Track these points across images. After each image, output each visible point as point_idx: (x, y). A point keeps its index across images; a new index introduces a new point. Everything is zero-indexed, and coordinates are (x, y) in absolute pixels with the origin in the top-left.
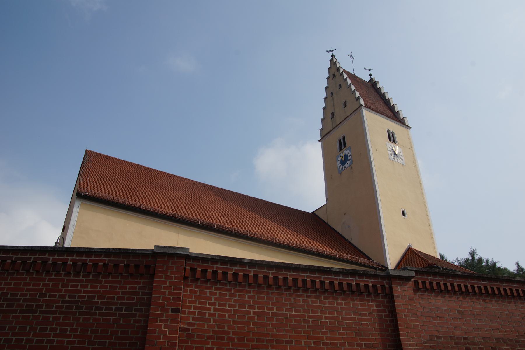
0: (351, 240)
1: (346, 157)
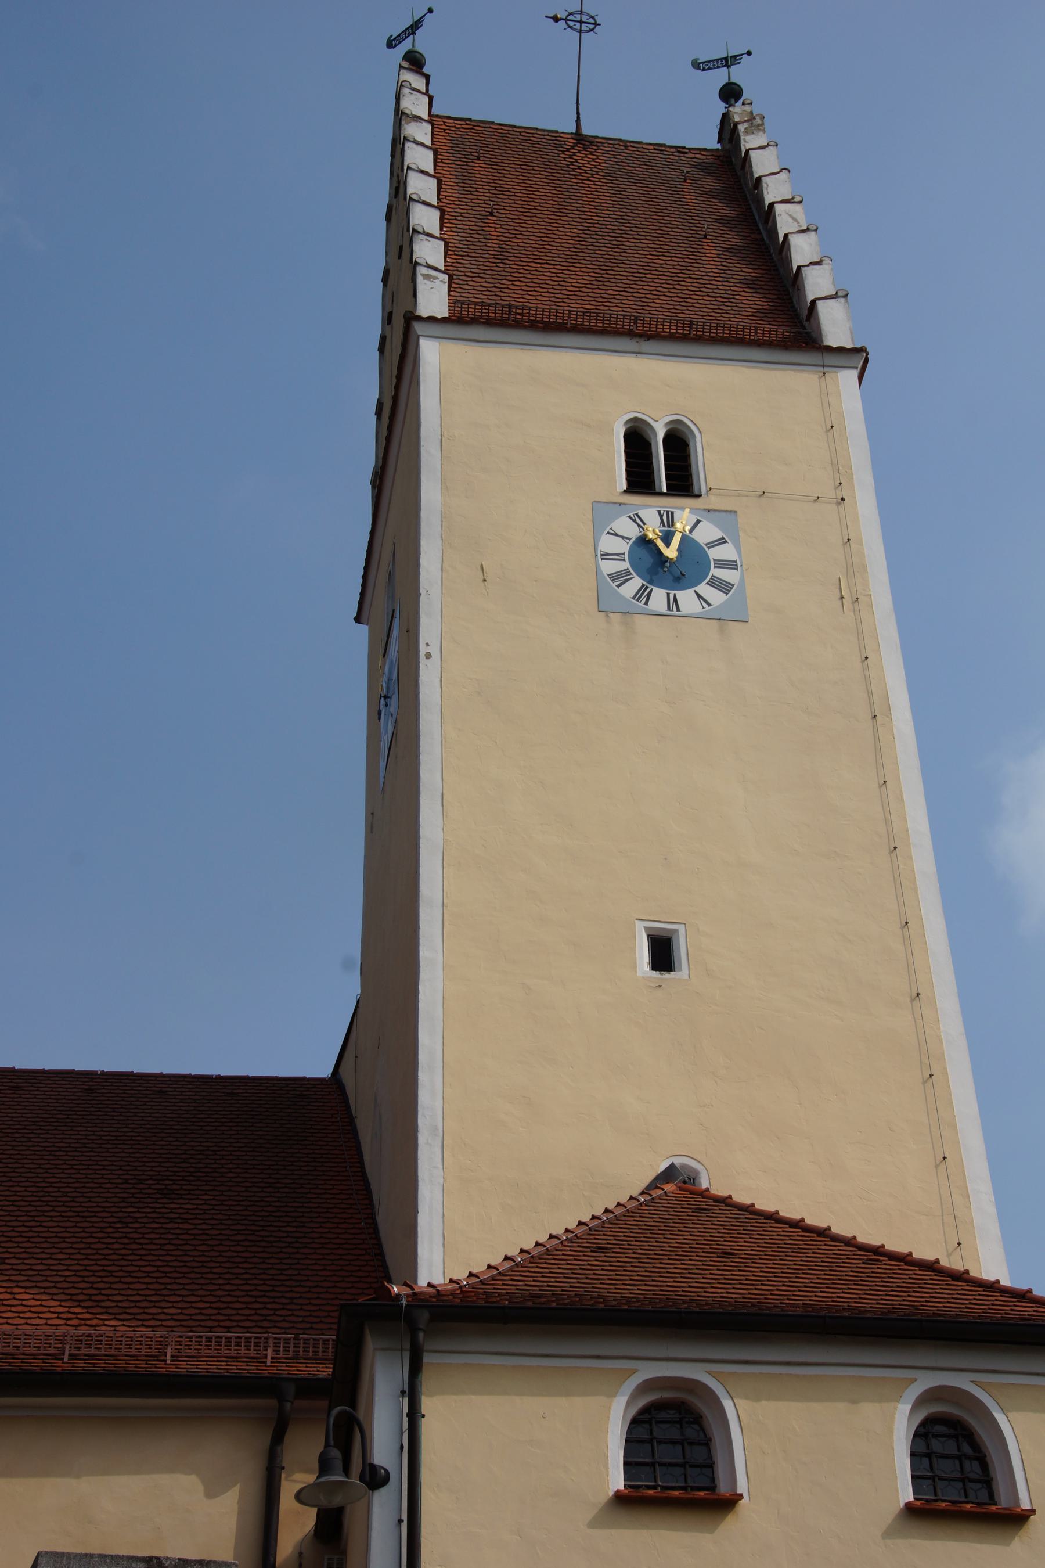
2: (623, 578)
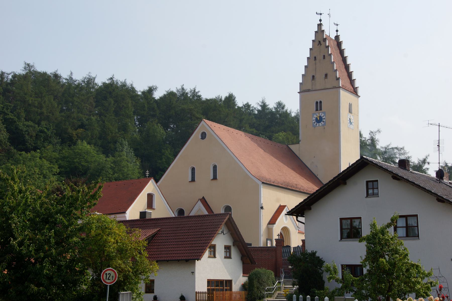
0: (317, 175)
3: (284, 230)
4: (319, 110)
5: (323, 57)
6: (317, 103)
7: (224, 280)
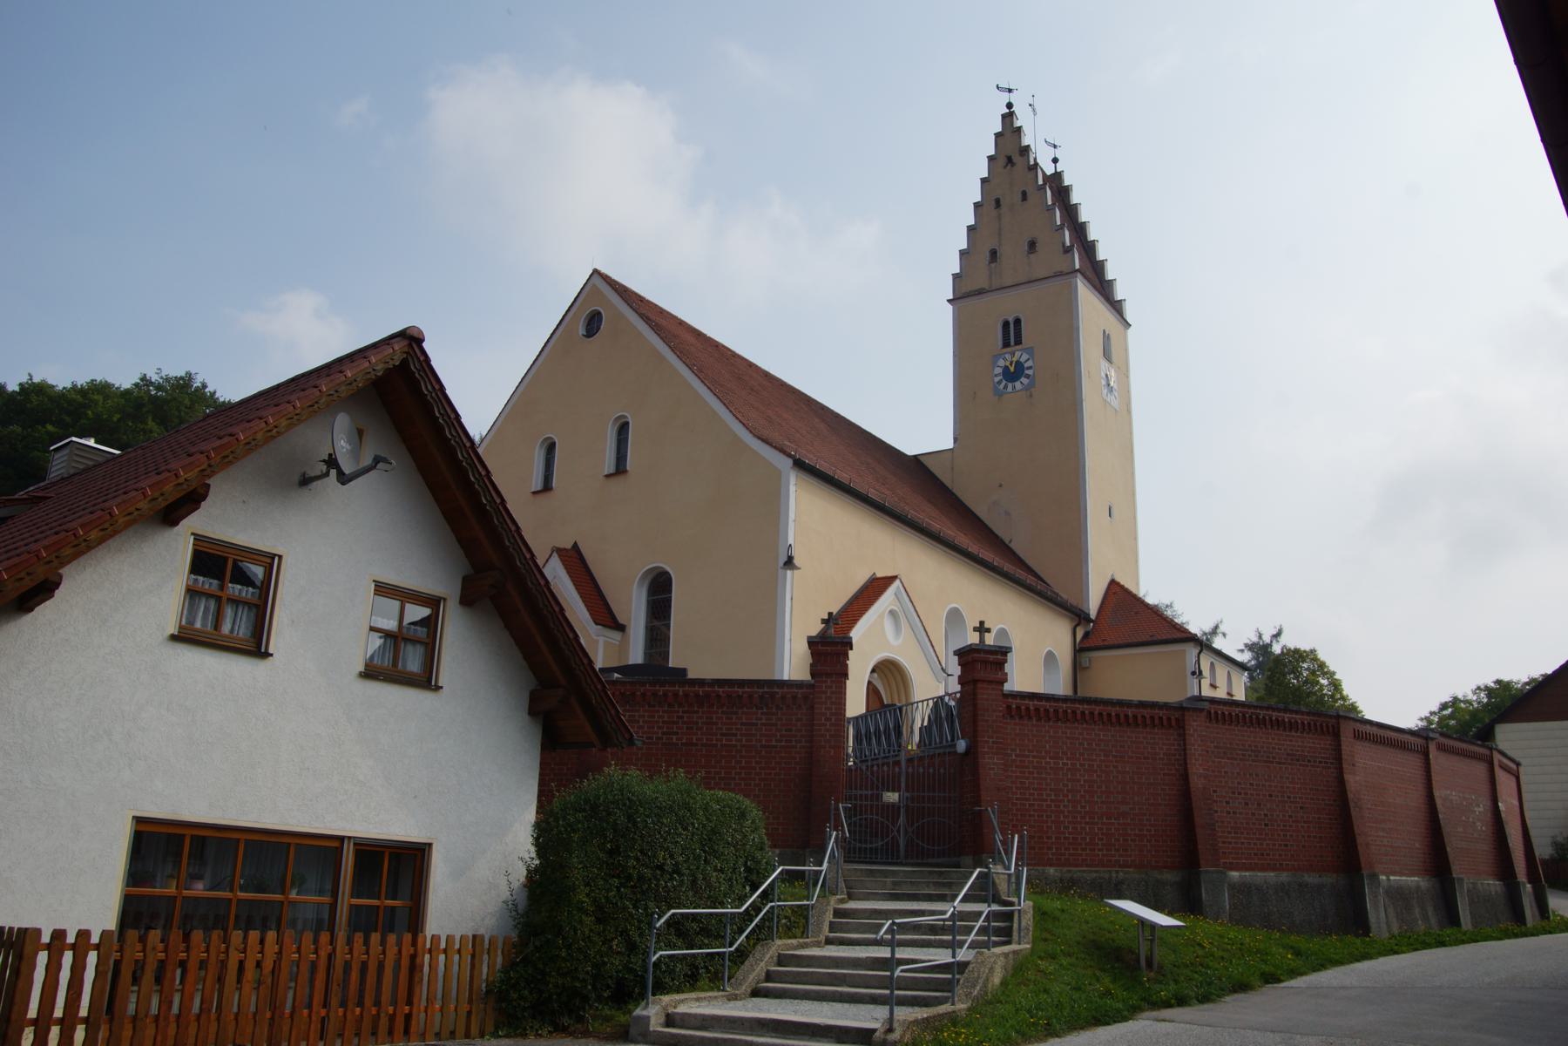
0: (1010, 542)
1: (1019, 367)
2: (1000, 382)
3: (888, 680)
4: (1012, 342)
5: (1020, 196)
6: (1006, 324)
7: (341, 839)
